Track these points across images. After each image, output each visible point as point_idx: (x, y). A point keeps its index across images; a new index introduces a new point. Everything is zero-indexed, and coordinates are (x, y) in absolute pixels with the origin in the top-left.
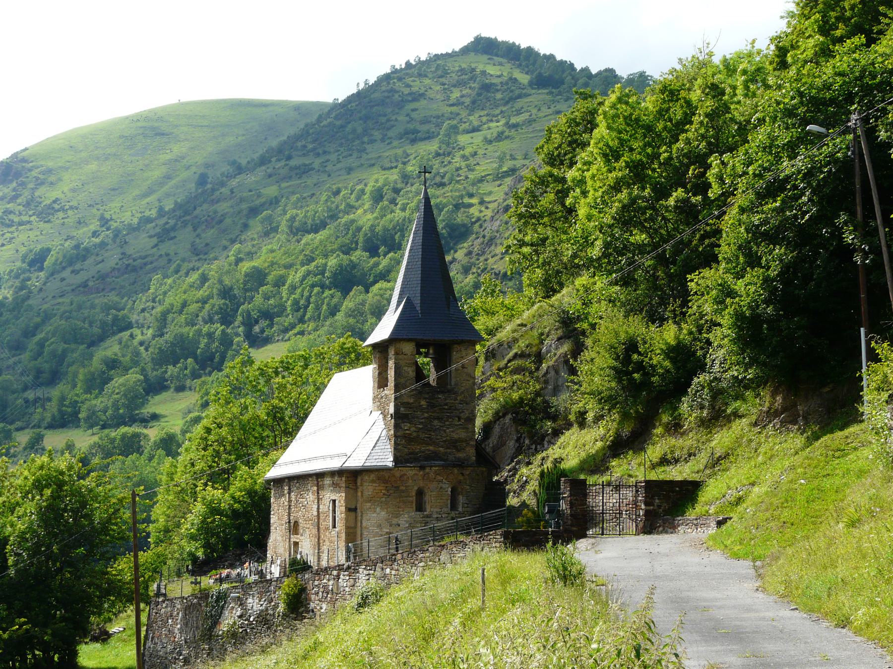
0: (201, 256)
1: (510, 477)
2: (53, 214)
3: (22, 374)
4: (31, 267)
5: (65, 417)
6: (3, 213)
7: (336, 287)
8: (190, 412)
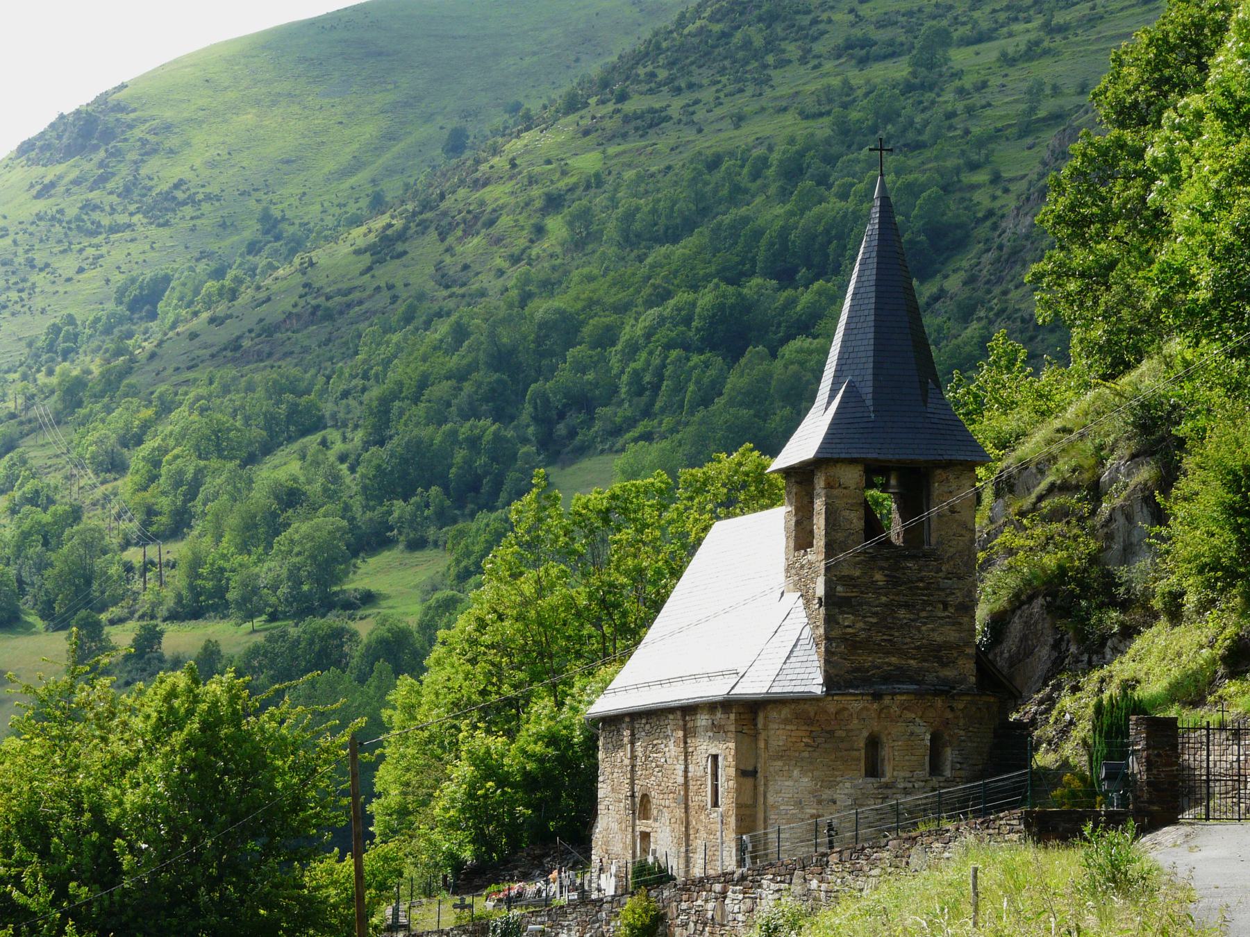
0: (454, 289)
1: (1042, 714)
2: (174, 210)
3: (119, 517)
4: (133, 313)
5: (202, 598)
6: (81, 208)
7: (713, 348)
8: (435, 589)
